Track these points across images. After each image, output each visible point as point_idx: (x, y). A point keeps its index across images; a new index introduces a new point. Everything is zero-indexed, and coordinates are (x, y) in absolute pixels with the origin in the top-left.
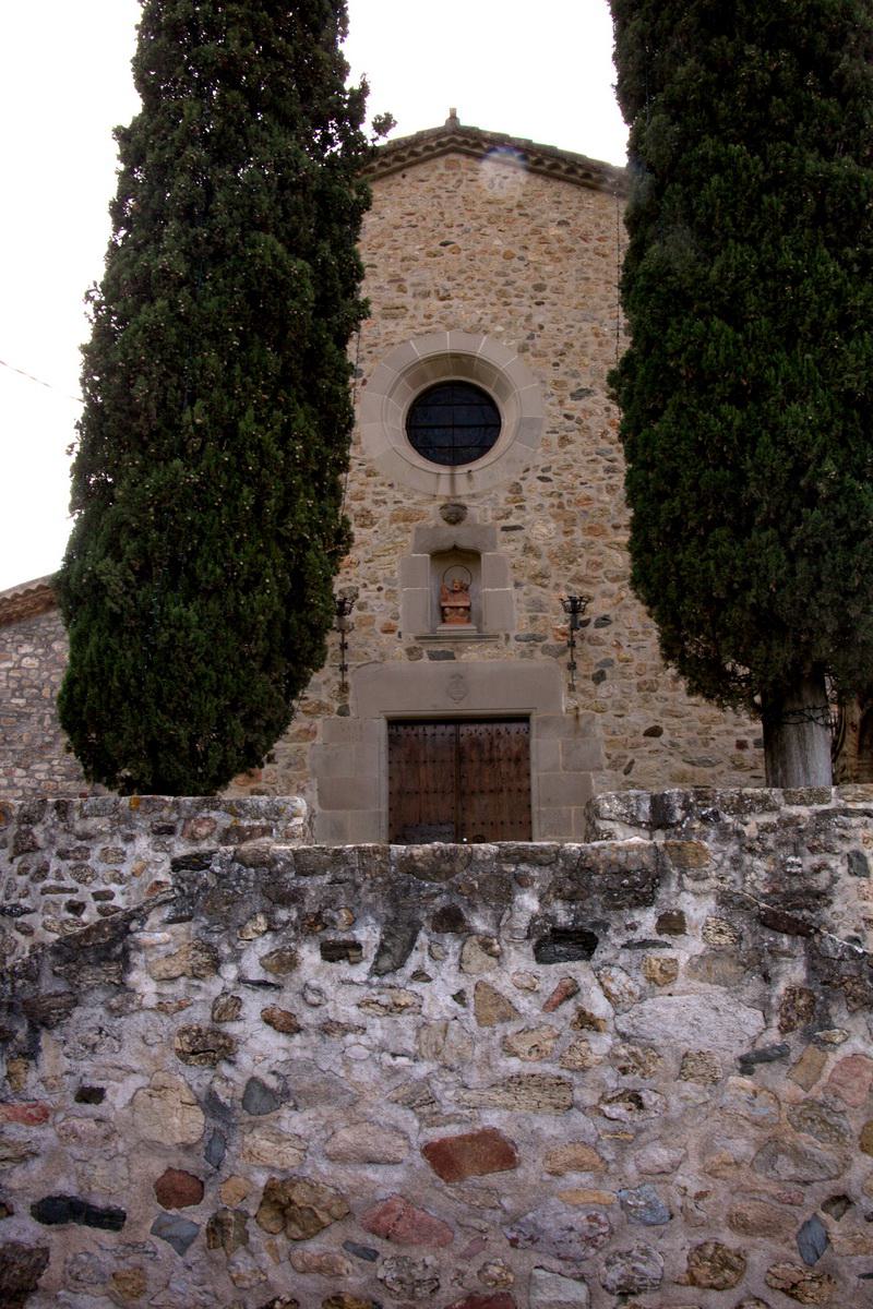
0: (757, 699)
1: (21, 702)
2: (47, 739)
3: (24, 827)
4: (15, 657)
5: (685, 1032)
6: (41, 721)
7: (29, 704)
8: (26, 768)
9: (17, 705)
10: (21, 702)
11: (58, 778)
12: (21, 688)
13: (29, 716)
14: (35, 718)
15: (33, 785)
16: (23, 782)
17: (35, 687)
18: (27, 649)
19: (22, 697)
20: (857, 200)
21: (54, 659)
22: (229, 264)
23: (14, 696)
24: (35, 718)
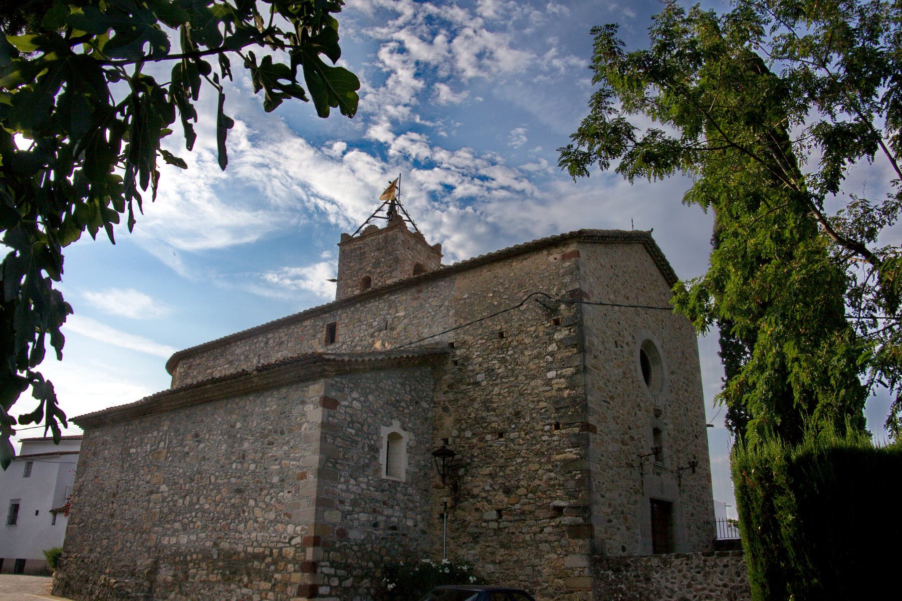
0: (141, 94)
1: (353, 431)
2: (367, 461)
3: (273, 581)
4: (349, 399)
5: (369, 107)
6: (363, 448)
7: (356, 434)
8: (356, 480)
9: (351, 433)
10: (353, 431)
11: (372, 489)
12: (352, 422)
13: (357, 443)
14: (360, 446)
15: (359, 491)
16: (354, 489)
17: (359, 423)
18: (355, 395)
19: (352, 428)
20: (259, 571)
21: (368, 407)
22: (485, 366)
23: (349, 427)
24: (360, 446)
